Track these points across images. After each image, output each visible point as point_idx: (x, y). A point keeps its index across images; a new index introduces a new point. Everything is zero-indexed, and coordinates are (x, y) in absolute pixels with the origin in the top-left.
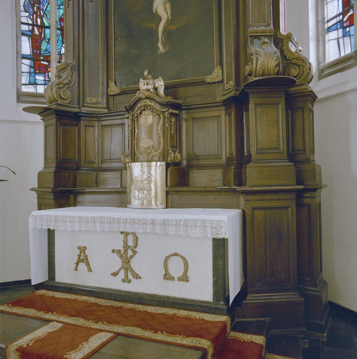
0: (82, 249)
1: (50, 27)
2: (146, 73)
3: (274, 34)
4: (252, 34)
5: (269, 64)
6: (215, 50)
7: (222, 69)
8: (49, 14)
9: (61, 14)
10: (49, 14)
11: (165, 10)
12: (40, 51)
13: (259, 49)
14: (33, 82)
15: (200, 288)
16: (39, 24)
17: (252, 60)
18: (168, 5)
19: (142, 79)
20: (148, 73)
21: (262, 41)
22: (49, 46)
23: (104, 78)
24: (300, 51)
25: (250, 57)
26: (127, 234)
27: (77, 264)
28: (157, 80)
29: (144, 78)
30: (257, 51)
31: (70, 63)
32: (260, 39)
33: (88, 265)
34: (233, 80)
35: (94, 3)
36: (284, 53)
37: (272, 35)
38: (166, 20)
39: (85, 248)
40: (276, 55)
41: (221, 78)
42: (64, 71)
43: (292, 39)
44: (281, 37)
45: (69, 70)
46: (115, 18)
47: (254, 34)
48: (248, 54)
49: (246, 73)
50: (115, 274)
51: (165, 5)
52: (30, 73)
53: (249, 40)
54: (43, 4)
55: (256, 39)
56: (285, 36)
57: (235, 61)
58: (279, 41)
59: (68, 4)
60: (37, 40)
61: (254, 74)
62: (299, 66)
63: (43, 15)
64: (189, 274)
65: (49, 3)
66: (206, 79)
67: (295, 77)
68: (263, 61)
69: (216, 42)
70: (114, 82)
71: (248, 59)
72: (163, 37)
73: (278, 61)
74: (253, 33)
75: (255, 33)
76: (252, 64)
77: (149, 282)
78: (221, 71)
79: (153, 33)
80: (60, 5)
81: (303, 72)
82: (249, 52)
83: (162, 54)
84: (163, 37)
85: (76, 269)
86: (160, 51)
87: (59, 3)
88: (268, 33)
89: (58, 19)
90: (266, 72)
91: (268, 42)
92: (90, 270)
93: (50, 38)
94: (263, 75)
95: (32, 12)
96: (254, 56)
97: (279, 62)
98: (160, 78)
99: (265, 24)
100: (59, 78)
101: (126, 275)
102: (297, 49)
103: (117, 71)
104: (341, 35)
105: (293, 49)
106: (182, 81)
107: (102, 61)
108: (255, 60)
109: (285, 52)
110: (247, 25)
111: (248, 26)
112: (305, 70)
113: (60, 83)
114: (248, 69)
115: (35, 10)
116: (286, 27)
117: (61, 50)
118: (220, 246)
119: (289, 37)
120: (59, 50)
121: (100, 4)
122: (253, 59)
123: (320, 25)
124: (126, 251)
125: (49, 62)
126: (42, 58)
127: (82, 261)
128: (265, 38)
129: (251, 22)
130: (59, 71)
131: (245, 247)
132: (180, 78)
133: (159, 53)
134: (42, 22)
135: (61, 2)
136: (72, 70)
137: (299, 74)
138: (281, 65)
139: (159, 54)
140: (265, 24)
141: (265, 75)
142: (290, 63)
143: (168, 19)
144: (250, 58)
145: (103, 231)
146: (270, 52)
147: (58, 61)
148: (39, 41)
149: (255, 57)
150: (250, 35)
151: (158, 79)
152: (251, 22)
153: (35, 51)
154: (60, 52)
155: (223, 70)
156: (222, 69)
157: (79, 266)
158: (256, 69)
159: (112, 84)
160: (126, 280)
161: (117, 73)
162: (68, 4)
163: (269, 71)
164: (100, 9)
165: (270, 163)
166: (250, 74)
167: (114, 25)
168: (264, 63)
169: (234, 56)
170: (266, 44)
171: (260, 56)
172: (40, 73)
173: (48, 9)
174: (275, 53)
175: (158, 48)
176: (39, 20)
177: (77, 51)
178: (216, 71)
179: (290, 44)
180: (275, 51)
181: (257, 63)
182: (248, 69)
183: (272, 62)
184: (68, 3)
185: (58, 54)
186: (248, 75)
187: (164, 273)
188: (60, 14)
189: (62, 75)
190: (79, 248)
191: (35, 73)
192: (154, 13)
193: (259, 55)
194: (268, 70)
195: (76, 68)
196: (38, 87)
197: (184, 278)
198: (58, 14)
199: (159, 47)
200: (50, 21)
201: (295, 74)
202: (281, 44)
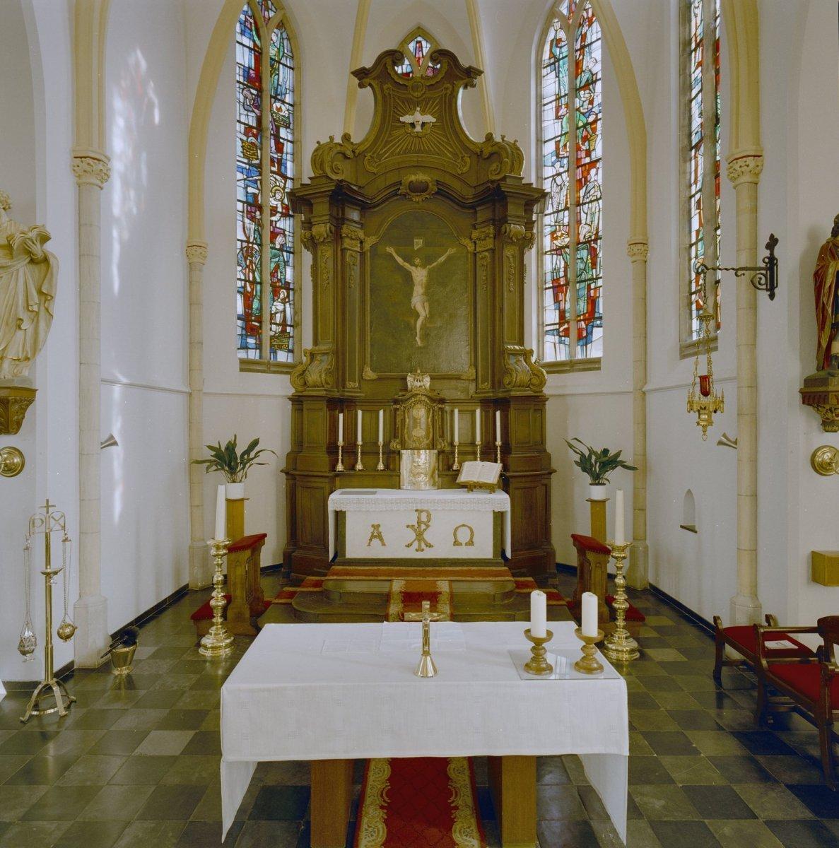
0: (376, 527)
11: (424, 307)
12: (252, 310)
14: (244, 346)
15: (484, 549)
16: (251, 279)
18: (426, 304)
26: (422, 511)
27: (371, 540)
33: (381, 539)
39: (379, 526)
50: (409, 546)
52: (242, 335)
60: (249, 297)
64: (475, 540)
77: (441, 548)
79: (412, 329)
85: (369, 545)
92: (384, 544)
95: (245, 266)
101: (420, 546)
104: (557, 341)
106: (484, 397)
115: (248, 264)
118: (499, 517)
123: (541, 329)
124: (419, 526)
125: (260, 322)
126: (253, 318)
127: (375, 537)
131: (47, 555)
134: (254, 277)
145: (392, 510)
148: (251, 299)
153: (247, 310)
157: (372, 543)
159: (368, 369)
160: (419, 550)
165: (439, 430)
172: (251, 336)
176: (251, 275)
187: (454, 540)
190: (373, 526)
191: (247, 336)
196: (250, 351)
197: (471, 543)
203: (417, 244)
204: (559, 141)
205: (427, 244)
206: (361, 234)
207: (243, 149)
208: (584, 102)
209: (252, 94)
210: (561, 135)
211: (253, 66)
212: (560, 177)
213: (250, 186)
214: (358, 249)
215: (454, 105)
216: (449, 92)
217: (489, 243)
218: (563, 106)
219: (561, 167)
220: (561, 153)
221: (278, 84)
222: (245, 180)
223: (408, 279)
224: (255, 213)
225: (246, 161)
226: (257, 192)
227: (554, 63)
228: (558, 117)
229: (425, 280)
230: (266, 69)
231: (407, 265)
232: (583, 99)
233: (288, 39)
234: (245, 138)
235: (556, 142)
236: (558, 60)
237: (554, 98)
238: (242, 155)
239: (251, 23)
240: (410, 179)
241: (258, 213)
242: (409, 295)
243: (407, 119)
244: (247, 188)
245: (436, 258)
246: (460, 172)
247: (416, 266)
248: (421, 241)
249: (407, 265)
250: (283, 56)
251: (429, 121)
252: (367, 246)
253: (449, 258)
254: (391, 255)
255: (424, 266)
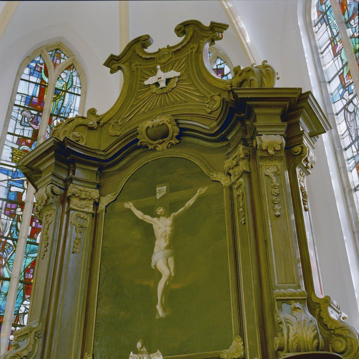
1: (11, 280)
2: (139, 345)
3: (307, 298)
4: (279, 298)
5: (305, 335)
6: (232, 315)
7: (243, 340)
8: (12, 264)
9: (27, 264)
10: (12, 264)
11: (167, 265)
13: (289, 316)
17: (282, 330)
18: (171, 260)
19: (133, 353)
20: (142, 345)
21: (292, 306)
22: (4, 302)
23: (78, 350)
24: (344, 318)
25: (278, 325)
28: (153, 355)
29: (136, 352)
30: (287, 319)
31: (34, 328)
32: (289, 304)
34: (259, 356)
35: (76, 254)
36: (324, 321)
37: (305, 299)
38: (168, 276)
40: (312, 325)
41: (243, 353)
42: (24, 339)
43: (332, 303)
44: (317, 301)
45: (31, 337)
46: (101, 272)
47: (282, 298)
48: (276, 322)
49: (275, 347)
51: (167, 260)
53: (276, 304)
54: (8, 251)
55: (285, 303)
56: (322, 299)
57: (260, 331)
58: (316, 307)
59: (44, 255)
61: (286, 349)
62: (345, 338)
63: (5, 264)
65: (15, 251)
66: (221, 355)
67: (341, 353)
68: (296, 332)
69: (233, 305)
70: (92, 355)
71: (277, 328)
72: (163, 298)
73: (316, 331)
74: (281, 297)
75: (283, 297)
76: (283, 335)
78: (242, 343)
79: (151, 293)
80: (29, 253)
81: (352, 346)
82: (277, 319)
83: (161, 319)
84: (163, 298)
86: (159, 315)
87: (28, 251)
88: (299, 296)
89: (22, 270)
90: (302, 347)
91: (300, 307)
93: (8, 293)
94: (298, 350)
96: (284, 325)
97: (317, 333)
98: (158, 352)
99: (295, 285)
100: (17, 348)
102: (340, 317)
103: (97, 340)
105: (334, 315)
107: (78, 326)
108: (286, 331)
109: (324, 320)
110: (272, 286)
111: (273, 287)
112: (354, 344)
113: (16, 355)
114: (277, 341)
116: (323, 288)
117: (19, 309)
119: (327, 301)
120: (17, 309)
121: (84, 256)
122: (282, 329)
128: (296, 302)
129: (276, 283)
130: (18, 338)
132: (185, 353)
133: (157, 318)
135: (30, 249)
136: (36, 338)
137: (347, 349)
138: (320, 336)
139: (157, 319)
140: (295, 285)
141: (301, 351)
142: (333, 334)
143: (170, 276)
144: (279, 327)
146: (304, 320)
147: (13, 323)
149: (285, 326)
150: (277, 298)
151: (155, 354)
152: (276, 283)
154: (18, 311)
155: (244, 342)
156: (243, 340)
158: (288, 342)
161: (97, 343)
162: (44, 255)
163: (306, 346)
164: (83, 262)
166: (281, 349)
167: (99, 281)
168: (297, 335)
169: (258, 323)
170: (298, 310)
171: (292, 325)
173: (13, 257)
174: (311, 321)
175: (156, 311)
177: (46, 312)
178: (234, 343)
179: (330, 309)
180: (310, 319)
181: (288, 334)
182: (278, 342)
183: (309, 333)
184: (43, 254)
185: (15, 314)
186: (278, 350)
188: (26, 263)
189: (20, 344)
192: (153, 268)
193: (290, 324)
194: (305, 344)
195: (42, 335)
198: (24, 263)
199: (157, 310)
200: (11, 271)
201: (342, 349)
202: (318, 310)
203: (160, 191)
204: (343, 73)
205: (171, 190)
206: (95, 193)
207: (13, 155)
208: (355, 27)
209: (32, 114)
210: (343, 68)
211: (37, 95)
212: (351, 104)
213: (13, 186)
214: (91, 210)
215: (200, 58)
216: (194, 50)
217: (243, 166)
218: (339, 43)
219: (349, 94)
220: (346, 82)
221: (62, 106)
222: (9, 180)
223: (149, 232)
224: (15, 209)
225: (14, 165)
226: (22, 190)
227: (323, 17)
228: (335, 55)
229: (169, 230)
230: (49, 96)
231: (148, 218)
232: (354, 26)
233: (78, 76)
234: (16, 147)
235: (339, 76)
236: (326, 13)
237: (329, 42)
238: (10, 160)
239: (41, 68)
240: (146, 126)
241: (19, 209)
242: (151, 251)
243: (151, 81)
244: (10, 188)
245: (182, 203)
246: (209, 111)
247: (158, 216)
248: (165, 187)
249: (148, 218)
250: (71, 87)
251: (173, 76)
252: (102, 207)
253: (200, 199)
254: (129, 210)
255: (167, 215)
